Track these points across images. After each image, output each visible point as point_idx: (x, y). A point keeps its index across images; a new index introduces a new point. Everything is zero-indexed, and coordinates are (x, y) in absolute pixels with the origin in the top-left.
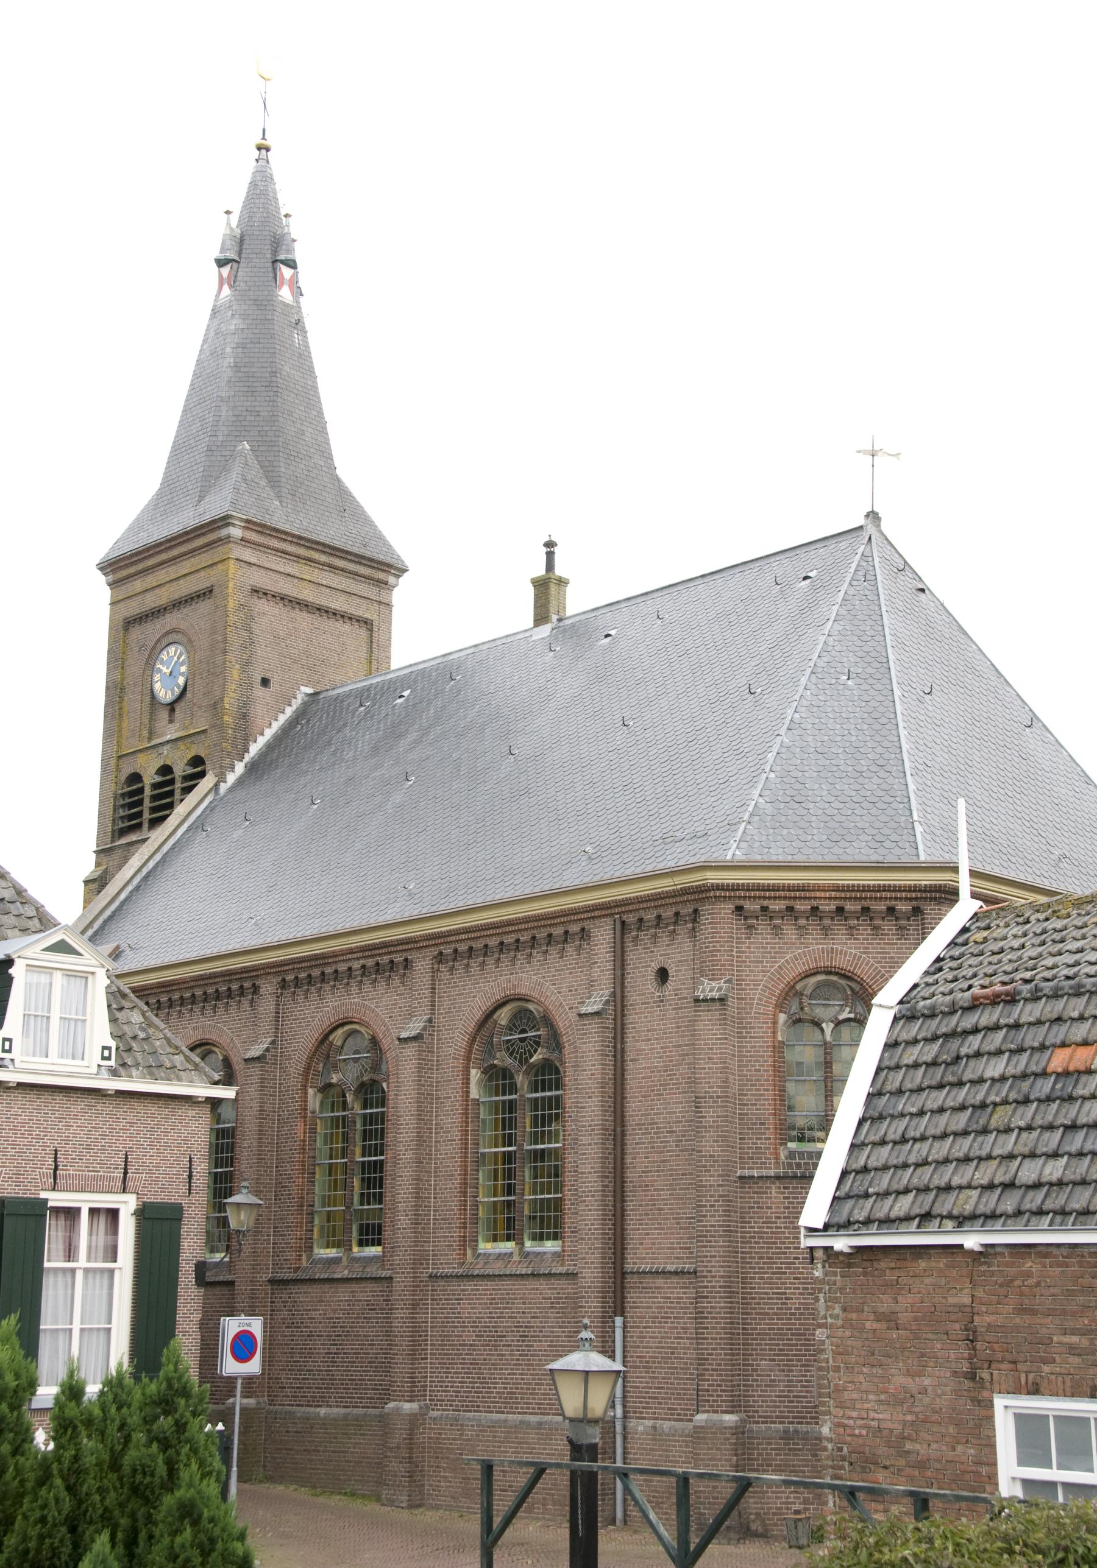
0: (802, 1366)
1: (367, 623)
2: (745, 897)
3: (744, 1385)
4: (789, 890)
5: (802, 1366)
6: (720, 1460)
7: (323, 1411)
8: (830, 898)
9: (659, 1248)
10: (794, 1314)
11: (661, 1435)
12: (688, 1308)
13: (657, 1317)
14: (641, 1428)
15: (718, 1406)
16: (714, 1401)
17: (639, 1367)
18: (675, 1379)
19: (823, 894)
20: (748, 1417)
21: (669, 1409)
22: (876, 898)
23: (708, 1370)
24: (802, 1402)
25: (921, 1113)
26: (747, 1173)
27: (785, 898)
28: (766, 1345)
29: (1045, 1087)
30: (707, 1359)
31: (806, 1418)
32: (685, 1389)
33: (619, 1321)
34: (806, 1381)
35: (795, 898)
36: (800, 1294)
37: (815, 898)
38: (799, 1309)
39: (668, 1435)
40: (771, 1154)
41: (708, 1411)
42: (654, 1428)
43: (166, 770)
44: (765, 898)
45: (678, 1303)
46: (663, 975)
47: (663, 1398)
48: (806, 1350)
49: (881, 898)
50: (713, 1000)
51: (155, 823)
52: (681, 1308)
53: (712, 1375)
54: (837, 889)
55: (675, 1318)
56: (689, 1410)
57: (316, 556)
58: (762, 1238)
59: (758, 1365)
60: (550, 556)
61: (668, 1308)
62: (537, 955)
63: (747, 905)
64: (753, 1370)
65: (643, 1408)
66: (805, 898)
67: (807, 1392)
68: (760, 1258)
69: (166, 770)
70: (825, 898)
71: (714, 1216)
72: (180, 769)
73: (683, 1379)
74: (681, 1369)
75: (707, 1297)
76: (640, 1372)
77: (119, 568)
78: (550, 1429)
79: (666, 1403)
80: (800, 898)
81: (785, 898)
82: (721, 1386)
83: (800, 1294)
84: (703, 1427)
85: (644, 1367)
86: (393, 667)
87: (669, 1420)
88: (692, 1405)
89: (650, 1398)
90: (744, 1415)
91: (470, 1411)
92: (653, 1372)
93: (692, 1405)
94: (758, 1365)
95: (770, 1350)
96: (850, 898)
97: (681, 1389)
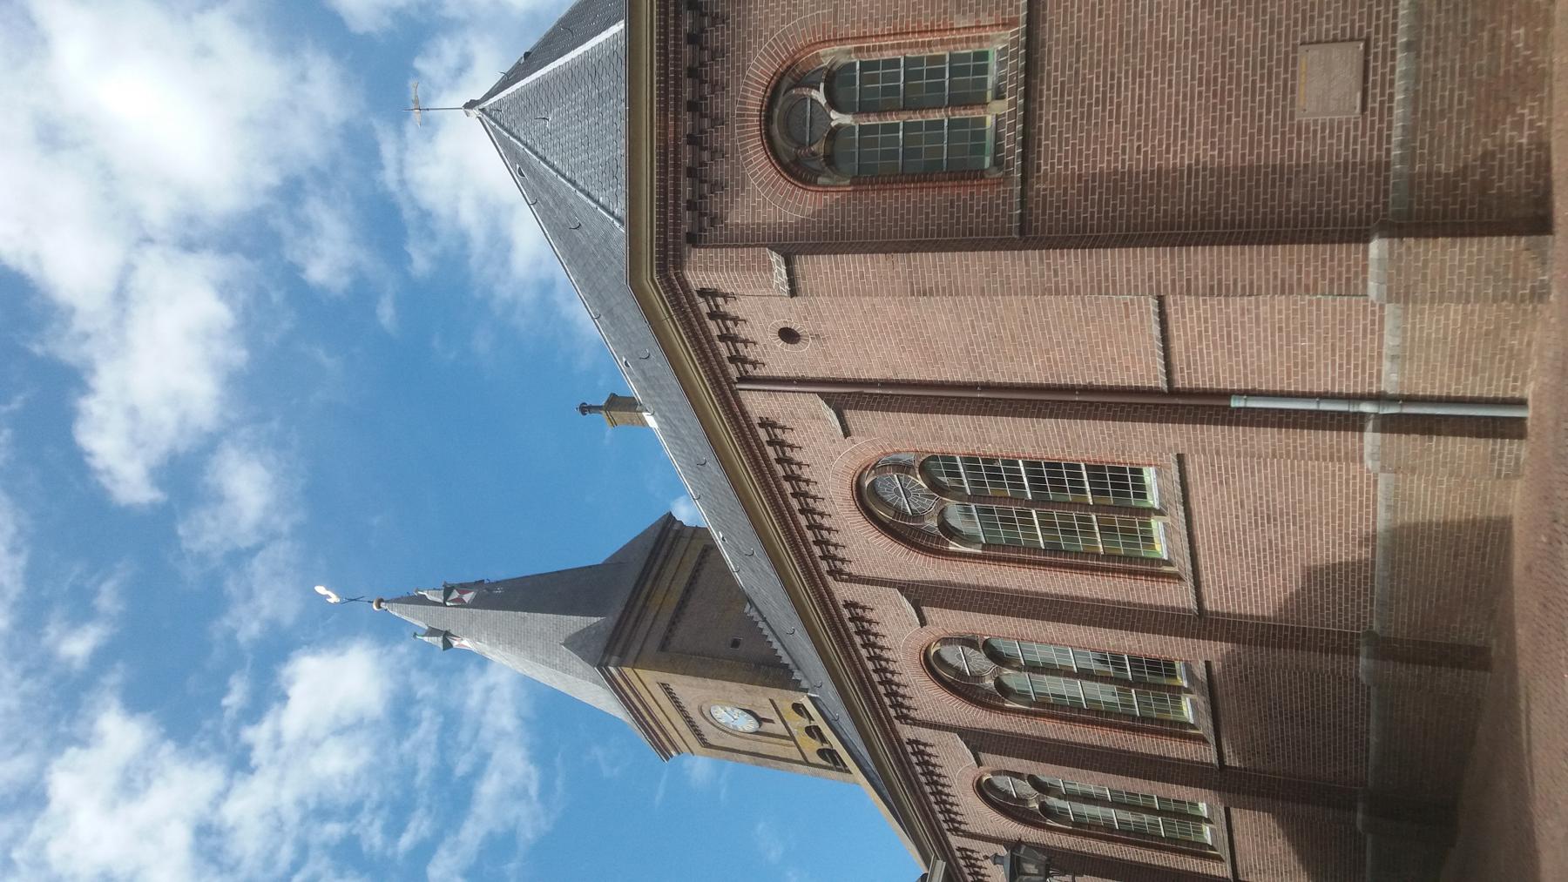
0: (1299, 138)
2: (675, 231)
3: (1327, 225)
4: (666, 173)
5: (1299, 138)
6: (1443, 262)
7: (1373, 739)
8: (676, 119)
9: (1131, 344)
10: (1220, 151)
11: (1404, 348)
12: (1212, 306)
13: (1230, 351)
14: (1394, 377)
15: (1356, 265)
16: (1348, 271)
17: (1304, 377)
18: (1318, 327)
19: (671, 129)
20: (1376, 218)
21: (1365, 336)
22: (675, 59)
23: (1299, 280)
24: (1355, 137)
26: (1015, 224)
27: (676, 179)
28: (1265, 193)
30: (1283, 281)
31: (1380, 130)
32: (1334, 314)
33: (1236, 403)
34: (1323, 131)
35: (676, 166)
36: (1191, 143)
37: (676, 139)
38: (1213, 144)
39: (1404, 339)
40: (992, 191)
41: (1365, 281)
42: (1393, 357)
44: (676, 205)
45: (1206, 321)
46: (788, 335)
47: (1349, 345)
48: (1275, 133)
49: (675, 52)
50: (790, 272)
52: (1213, 317)
53: (1308, 273)
54: (664, 111)
55: (1228, 326)
56: (1365, 308)
57: (645, 591)
58: (1107, 201)
59: (1296, 204)
61: (1214, 334)
62: (806, 473)
63: (685, 228)
64: (1304, 212)
65: (1364, 372)
66: (676, 153)
67: (1340, 130)
68: (1136, 204)
70: (676, 126)
71: (1070, 271)
73: (1318, 316)
74: (1303, 317)
75: (1188, 281)
76: (1311, 374)
78: (1396, 495)
79: (1356, 339)
80: (676, 159)
81: (676, 179)
82: (1324, 261)
83: (1191, 143)
84: (1389, 289)
85: (1303, 369)
87: (1381, 336)
88: (1357, 303)
89: (1348, 363)
90: (1373, 225)
91: (1373, 587)
92: (1311, 357)
93: (1357, 303)
94: (1296, 204)
95: (1273, 186)
96: (676, 93)
97: (1334, 318)
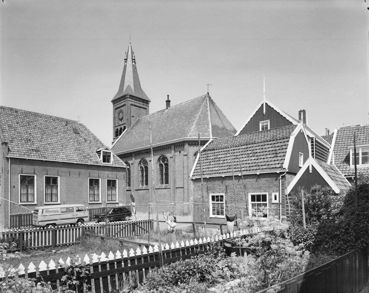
1: (146, 109)
25: (204, 163)
29: (216, 160)
43: (121, 128)
51: (120, 135)
60: (168, 97)
69: (121, 128)
72: (123, 128)
77: (114, 102)
86: (150, 114)
